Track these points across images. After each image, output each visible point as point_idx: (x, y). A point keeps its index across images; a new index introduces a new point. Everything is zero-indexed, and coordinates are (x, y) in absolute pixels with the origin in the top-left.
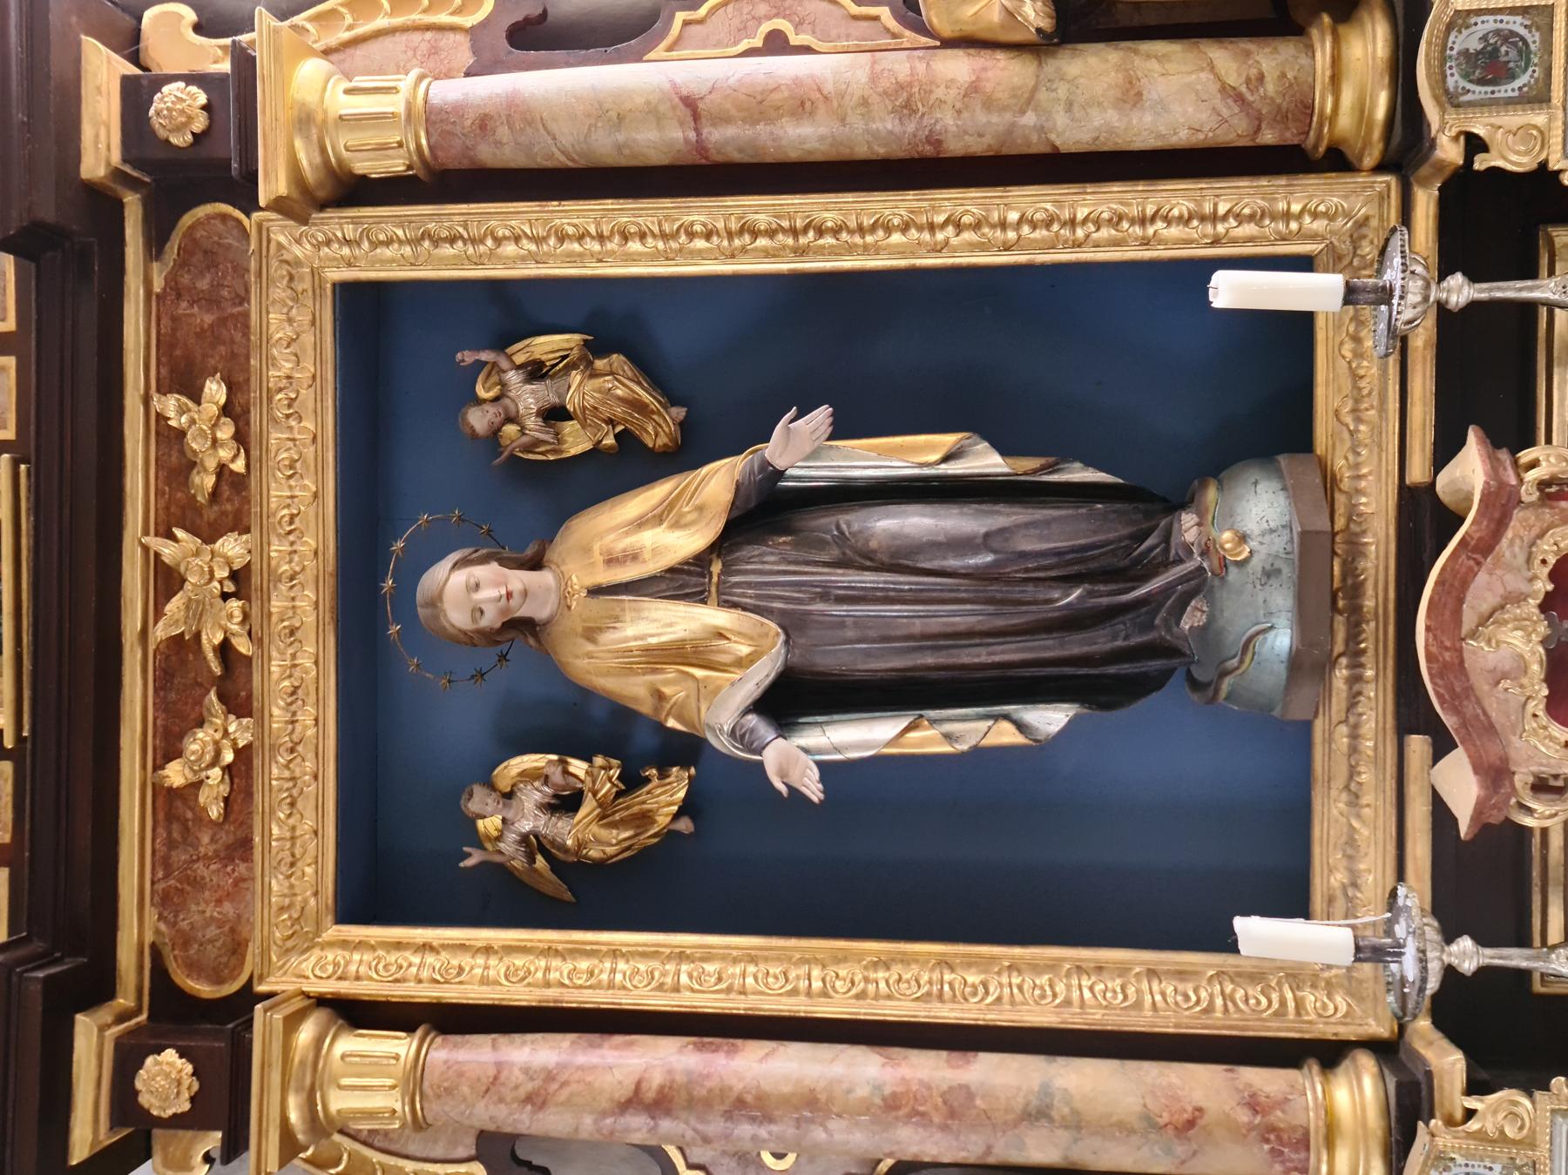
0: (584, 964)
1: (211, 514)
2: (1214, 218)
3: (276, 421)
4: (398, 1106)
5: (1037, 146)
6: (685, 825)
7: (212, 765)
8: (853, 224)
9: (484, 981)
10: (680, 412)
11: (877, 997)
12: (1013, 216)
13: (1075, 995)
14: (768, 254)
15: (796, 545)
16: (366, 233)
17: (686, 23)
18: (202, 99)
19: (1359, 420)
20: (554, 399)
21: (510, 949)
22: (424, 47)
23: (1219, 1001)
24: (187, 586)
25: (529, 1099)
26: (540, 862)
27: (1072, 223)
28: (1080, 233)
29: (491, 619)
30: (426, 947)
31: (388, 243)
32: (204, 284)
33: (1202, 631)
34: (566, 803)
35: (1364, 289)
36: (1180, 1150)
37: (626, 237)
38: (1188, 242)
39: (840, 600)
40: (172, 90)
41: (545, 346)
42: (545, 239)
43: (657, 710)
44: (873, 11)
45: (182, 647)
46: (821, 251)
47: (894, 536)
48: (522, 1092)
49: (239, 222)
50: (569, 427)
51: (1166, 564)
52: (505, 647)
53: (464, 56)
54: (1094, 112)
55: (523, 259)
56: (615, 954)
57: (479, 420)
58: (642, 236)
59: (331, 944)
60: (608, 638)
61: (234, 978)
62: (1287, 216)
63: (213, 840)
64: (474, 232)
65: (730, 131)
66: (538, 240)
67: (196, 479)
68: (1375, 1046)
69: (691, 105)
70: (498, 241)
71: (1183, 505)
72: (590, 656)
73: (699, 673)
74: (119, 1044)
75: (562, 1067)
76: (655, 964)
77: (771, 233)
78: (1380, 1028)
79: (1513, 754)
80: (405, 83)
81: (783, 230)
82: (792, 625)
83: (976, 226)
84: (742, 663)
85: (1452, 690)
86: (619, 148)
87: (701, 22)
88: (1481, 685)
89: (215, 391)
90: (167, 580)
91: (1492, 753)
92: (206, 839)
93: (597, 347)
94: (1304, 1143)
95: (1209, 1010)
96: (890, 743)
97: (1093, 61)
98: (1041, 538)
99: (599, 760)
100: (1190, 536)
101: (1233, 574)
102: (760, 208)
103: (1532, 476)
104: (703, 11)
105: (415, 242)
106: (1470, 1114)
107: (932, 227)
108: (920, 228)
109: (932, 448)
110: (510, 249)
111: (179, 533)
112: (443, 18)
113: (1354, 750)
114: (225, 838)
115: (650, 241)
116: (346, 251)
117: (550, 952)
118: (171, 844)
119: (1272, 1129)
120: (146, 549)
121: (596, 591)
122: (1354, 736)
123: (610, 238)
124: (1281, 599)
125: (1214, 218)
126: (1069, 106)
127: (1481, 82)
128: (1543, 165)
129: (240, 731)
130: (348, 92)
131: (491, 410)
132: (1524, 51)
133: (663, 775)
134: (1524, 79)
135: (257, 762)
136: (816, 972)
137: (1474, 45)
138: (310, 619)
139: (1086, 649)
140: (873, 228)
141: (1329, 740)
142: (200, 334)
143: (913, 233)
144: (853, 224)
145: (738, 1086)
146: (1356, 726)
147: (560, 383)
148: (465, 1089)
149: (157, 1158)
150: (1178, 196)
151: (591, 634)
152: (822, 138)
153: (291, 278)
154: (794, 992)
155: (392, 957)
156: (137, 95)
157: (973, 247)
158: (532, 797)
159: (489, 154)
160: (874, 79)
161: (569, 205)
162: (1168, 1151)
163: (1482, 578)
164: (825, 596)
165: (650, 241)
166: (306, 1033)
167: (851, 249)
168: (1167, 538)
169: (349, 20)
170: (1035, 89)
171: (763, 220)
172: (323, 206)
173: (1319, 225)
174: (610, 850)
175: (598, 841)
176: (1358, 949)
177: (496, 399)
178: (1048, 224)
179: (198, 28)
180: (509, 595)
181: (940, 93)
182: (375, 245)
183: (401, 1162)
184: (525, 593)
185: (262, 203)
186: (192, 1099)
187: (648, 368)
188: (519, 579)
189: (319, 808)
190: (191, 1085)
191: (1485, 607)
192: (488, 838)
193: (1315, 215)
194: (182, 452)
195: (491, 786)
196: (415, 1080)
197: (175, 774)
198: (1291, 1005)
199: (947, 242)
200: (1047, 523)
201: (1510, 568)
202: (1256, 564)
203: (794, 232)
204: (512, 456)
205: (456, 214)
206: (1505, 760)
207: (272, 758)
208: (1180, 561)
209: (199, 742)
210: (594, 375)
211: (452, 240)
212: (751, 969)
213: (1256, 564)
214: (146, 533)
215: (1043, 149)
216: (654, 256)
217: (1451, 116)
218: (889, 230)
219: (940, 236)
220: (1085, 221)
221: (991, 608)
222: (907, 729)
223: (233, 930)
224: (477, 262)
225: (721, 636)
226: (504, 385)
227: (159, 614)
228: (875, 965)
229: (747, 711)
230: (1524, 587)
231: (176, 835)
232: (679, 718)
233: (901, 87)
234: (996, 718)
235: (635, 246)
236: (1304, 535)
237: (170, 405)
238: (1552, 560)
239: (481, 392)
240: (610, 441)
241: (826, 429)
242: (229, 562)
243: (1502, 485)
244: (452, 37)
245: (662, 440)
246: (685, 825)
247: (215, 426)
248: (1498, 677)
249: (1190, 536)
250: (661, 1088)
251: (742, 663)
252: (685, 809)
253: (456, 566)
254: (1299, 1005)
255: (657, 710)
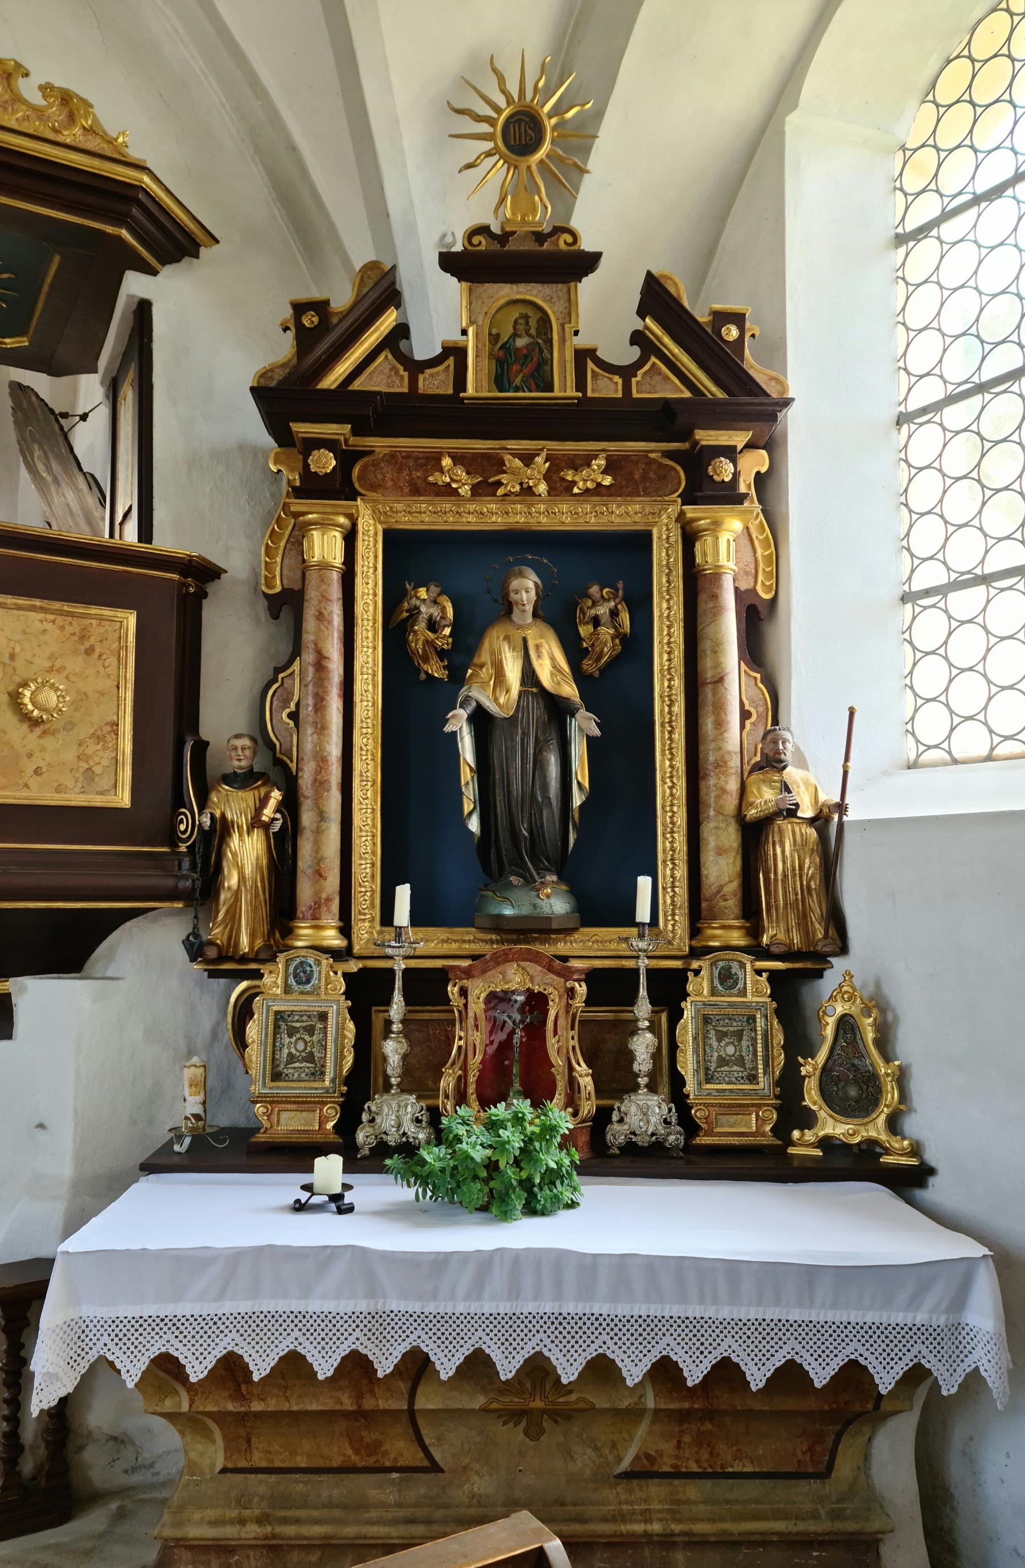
0: (370, 635)
1: (555, 477)
2: (673, 887)
3: (594, 507)
4: (315, 559)
5: (702, 817)
6: (423, 676)
7: (451, 478)
8: (673, 745)
9: (363, 594)
10: (597, 675)
11: (361, 755)
12: (675, 809)
13: (364, 834)
14: (662, 711)
15: (544, 722)
16: (671, 546)
17: (755, 678)
18: (727, 480)
19: (593, 942)
20: (603, 621)
21: (375, 603)
22: (748, 569)
23: (363, 889)
24: (526, 469)
25: (321, 614)
26: (405, 615)
27: (672, 832)
28: (668, 835)
29: (513, 597)
30: (376, 569)
31: (668, 555)
32: (652, 475)
33: (511, 884)
34: (433, 626)
35: (644, 930)
36: (309, 871)
37: (669, 653)
38: (664, 877)
39: (522, 740)
40: (730, 468)
41: (625, 618)
42: (669, 620)
43: (476, 665)
44: (759, 755)
45: (499, 466)
46: (663, 732)
47: (548, 761)
48: (323, 611)
49: (677, 490)
50: (590, 628)
51: (537, 869)
52: (500, 601)
53: (744, 586)
54: (714, 837)
55: (661, 611)
56: (375, 648)
57: (594, 590)
58: (669, 660)
59: (376, 528)
60: (506, 647)
61: (361, 486)
62: (673, 915)
63: (418, 477)
64: (672, 592)
65: (710, 696)
66: (668, 617)
67: (570, 472)
68: (350, 947)
69: (720, 680)
70: (668, 601)
71: (560, 878)
72: (498, 637)
73: (492, 683)
74: (337, 441)
75: (333, 626)
76: (370, 665)
77: (670, 712)
78: (356, 949)
79: (475, 980)
80: (731, 565)
81: (672, 716)
82: (512, 720)
83: (672, 795)
84: (496, 700)
85: (500, 957)
86: (704, 651)
87: (756, 684)
88: (499, 969)
89: (607, 481)
90: (528, 459)
91: (475, 973)
92: (418, 474)
93: (624, 639)
94: (315, 918)
95: (360, 885)
96: (464, 759)
97: (734, 837)
98: (548, 819)
99: (450, 640)
100: (548, 878)
101: (534, 893)
102: (679, 708)
103: (577, 984)
104: (760, 685)
105: (668, 565)
106: (336, 973)
107: (671, 777)
108: (671, 772)
109: (583, 777)
110: (665, 605)
111: (547, 465)
112: (760, 578)
113: (464, 941)
114: (419, 482)
115: (667, 663)
116: (664, 537)
117: (375, 621)
118: (416, 459)
119: (320, 907)
120: (542, 450)
121: (525, 641)
122: (469, 941)
123: (669, 647)
124: (526, 910)
125: (673, 887)
126: (716, 828)
127: (720, 973)
128: (689, 995)
129: (465, 490)
130: (728, 541)
131: (598, 596)
132: (731, 988)
133: (445, 667)
134: (720, 988)
135: (453, 498)
136: (370, 731)
137: (733, 971)
138: (511, 520)
139: (502, 840)
140: (671, 754)
141: (467, 933)
142: (631, 473)
143: (669, 770)
144: (673, 745)
145: (328, 698)
146: (473, 942)
147: (609, 624)
148: (324, 587)
149: (279, 450)
150: (682, 872)
151: (507, 638)
152: (706, 732)
153: (653, 514)
154: (362, 721)
155: (371, 555)
156: (730, 453)
157: (664, 793)
158: (435, 612)
159: (702, 597)
160: (729, 753)
161: (682, 630)
162: (309, 867)
163: (539, 968)
164: (524, 734)
165: (667, 663)
166: (342, 520)
167: (663, 745)
168: (547, 869)
169: (761, 537)
170: (723, 815)
171: (675, 709)
172: (683, 528)
173: (670, 927)
174: (413, 645)
175: (417, 641)
176: (400, 928)
177: (602, 596)
178: (672, 823)
179: (758, 473)
180: (524, 605)
181: (723, 778)
182: (667, 549)
183: (280, 556)
184: (524, 611)
185: (684, 507)
186: (316, 473)
187: (615, 661)
188: (529, 608)
189: (433, 523)
190: (322, 472)
191: (528, 969)
192: (416, 592)
193: (673, 926)
194: (582, 465)
195: (439, 595)
196: (325, 566)
197: (446, 462)
198: (363, 917)
199: (665, 783)
200: (554, 822)
201: (543, 978)
202: (538, 901)
203: (670, 722)
204: (578, 603)
205: (679, 583)
206: (473, 977)
207: (454, 505)
208: (538, 874)
209: (461, 473)
210: (613, 639)
211: (668, 581)
212: (370, 704)
213: (538, 901)
214: (548, 450)
215: (701, 819)
216: (661, 665)
217: (708, 963)
218: (671, 760)
219: (668, 780)
220: (673, 837)
221: (520, 799)
222: (470, 767)
223: (380, 485)
224: (660, 592)
225: (507, 692)
226: (609, 600)
227: (514, 455)
228: (373, 754)
229: (477, 702)
230: (536, 982)
231: (420, 461)
232: (472, 674)
233: (725, 763)
234: (475, 803)
235: (665, 657)
236: (550, 919)
237: (601, 462)
238: (546, 992)
239: (605, 590)
240: (585, 645)
241: (591, 734)
242: (536, 485)
243: (573, 973)
244: (752, 581)
245: (585, 667)
246: (423, 676)
247: (592, 480)
248: (504, 974)
249: (548, 878)
250: (327, 667)
251: (496, 700)
252: (430, 677)
253: (536, 583)
254: (364, 920)
255: (476, 665)
